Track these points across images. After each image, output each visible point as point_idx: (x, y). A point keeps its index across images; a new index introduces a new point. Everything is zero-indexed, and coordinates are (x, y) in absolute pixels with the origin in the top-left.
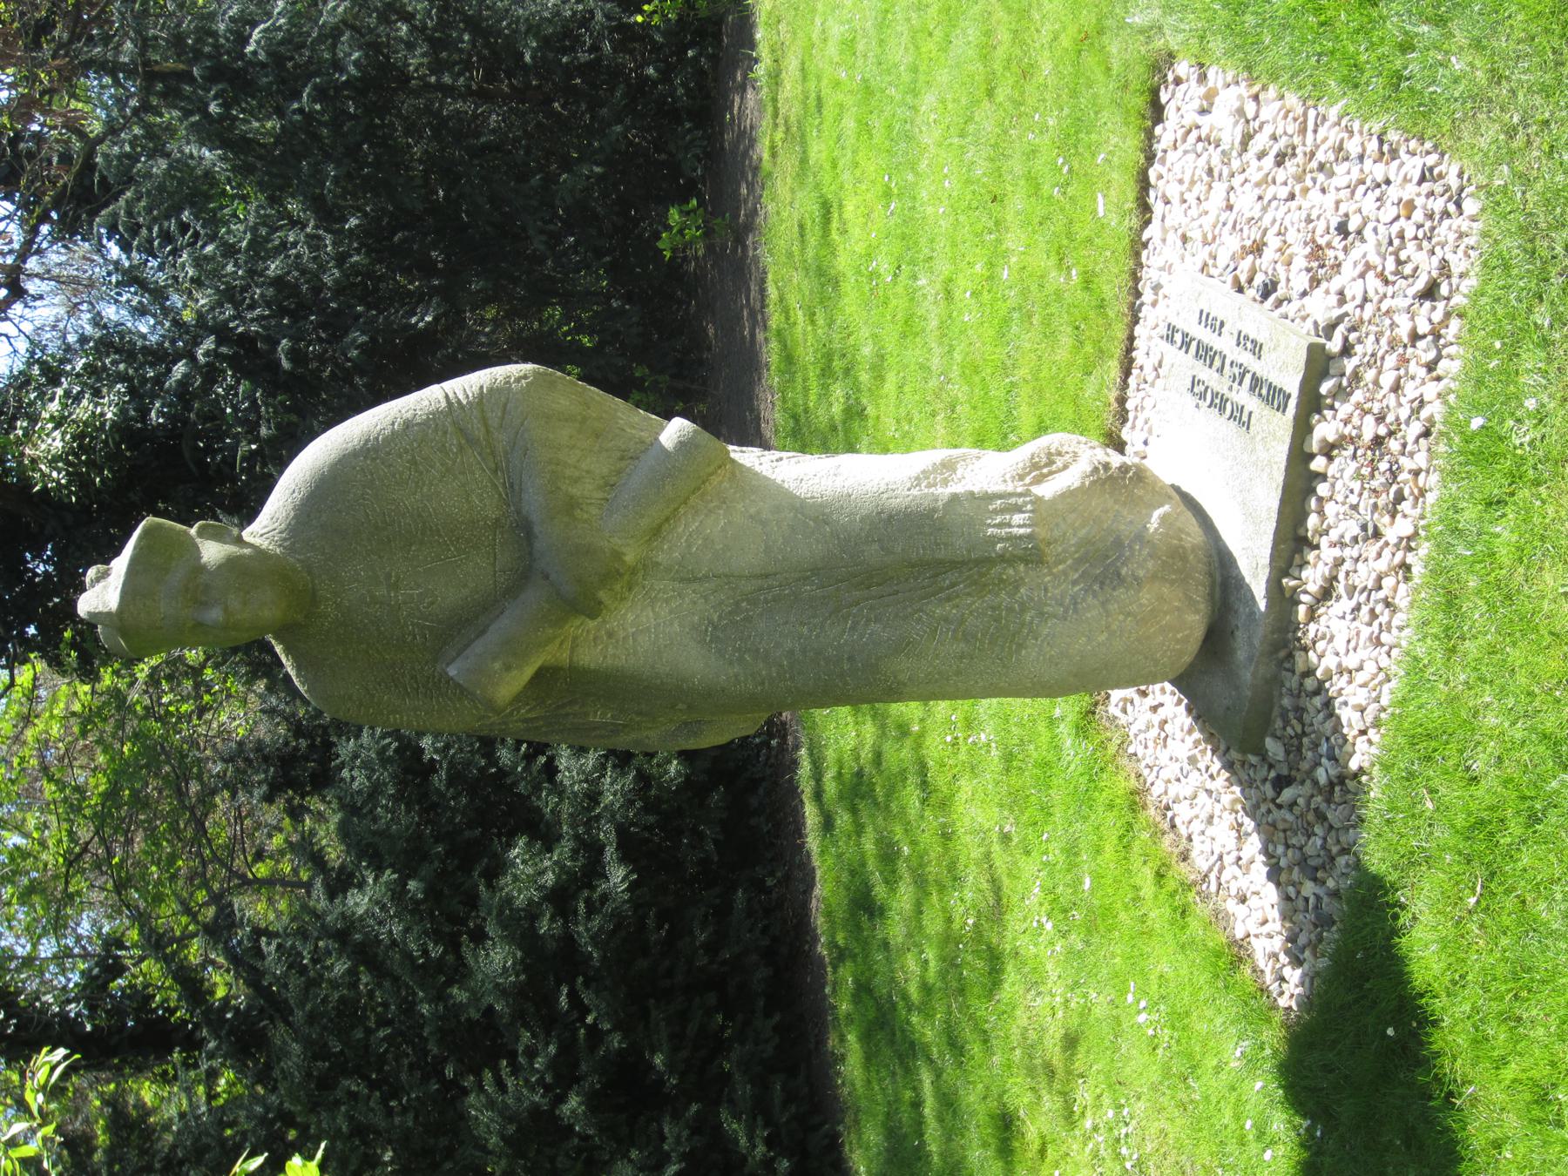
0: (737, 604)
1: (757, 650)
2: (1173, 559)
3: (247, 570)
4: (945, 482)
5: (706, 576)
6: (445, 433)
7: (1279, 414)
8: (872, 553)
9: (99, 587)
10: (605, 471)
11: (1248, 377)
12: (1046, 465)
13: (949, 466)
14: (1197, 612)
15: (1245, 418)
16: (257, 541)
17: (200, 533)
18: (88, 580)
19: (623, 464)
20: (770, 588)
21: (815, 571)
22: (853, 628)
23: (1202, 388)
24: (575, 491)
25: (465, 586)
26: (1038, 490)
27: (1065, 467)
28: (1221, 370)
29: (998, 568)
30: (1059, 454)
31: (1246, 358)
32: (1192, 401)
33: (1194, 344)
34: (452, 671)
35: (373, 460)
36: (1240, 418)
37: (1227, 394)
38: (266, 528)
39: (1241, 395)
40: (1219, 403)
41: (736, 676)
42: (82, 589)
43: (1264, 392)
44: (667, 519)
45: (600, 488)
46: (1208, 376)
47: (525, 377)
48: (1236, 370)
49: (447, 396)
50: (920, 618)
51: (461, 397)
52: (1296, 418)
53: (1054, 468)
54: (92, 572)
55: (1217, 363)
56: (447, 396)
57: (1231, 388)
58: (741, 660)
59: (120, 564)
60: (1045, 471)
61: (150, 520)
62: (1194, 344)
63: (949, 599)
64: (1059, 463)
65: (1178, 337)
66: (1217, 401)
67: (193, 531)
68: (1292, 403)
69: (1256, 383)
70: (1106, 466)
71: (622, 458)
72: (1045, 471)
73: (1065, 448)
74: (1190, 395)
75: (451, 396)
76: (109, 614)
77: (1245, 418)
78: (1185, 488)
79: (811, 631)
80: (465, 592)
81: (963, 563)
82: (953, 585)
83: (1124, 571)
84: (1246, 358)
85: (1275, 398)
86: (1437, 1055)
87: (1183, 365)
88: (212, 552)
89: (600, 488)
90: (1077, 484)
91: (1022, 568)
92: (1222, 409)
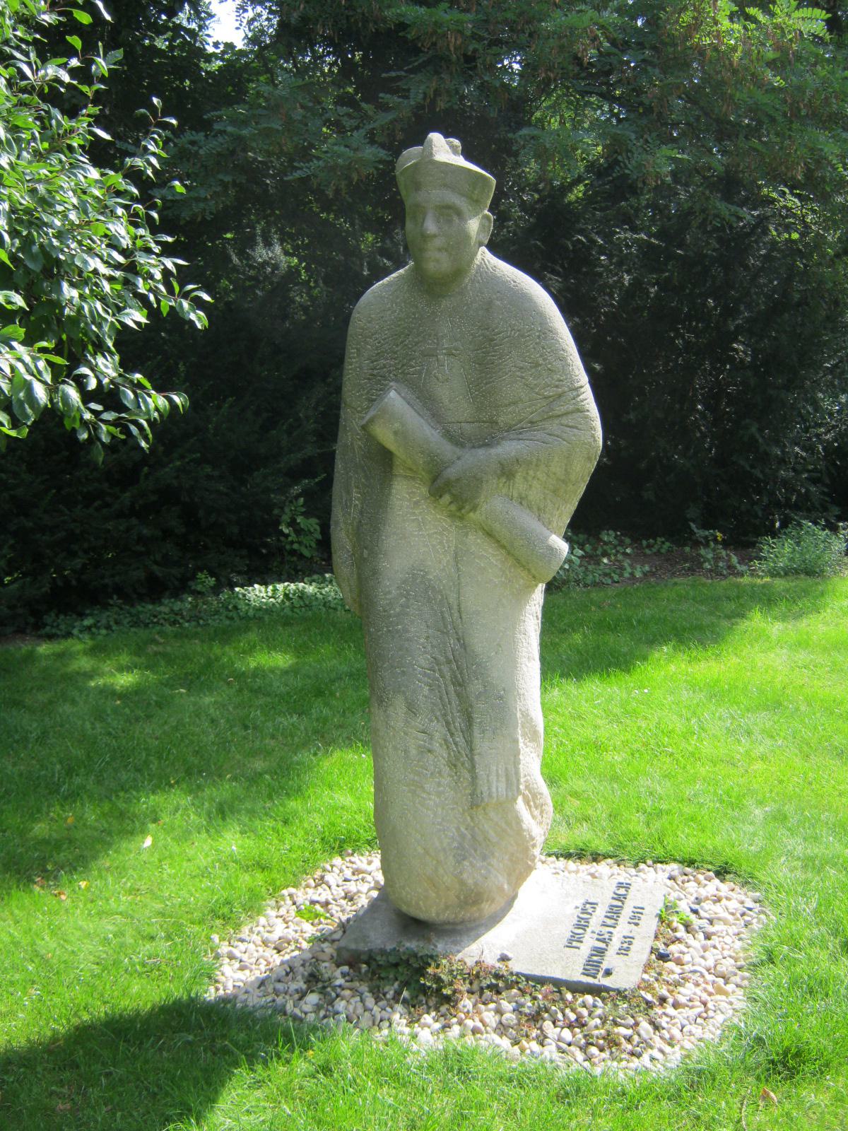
0: (440, 591)
1: (408, 607)
2: (473, 898)
3: (460, 246)
4: (524, 735)
5: (458, 569)
6: (557, 387)
7: (581, 971)
8: (475, 687)
9: (447, 147)
10: (531, 498)
11: (602, 945)
12: (535, 803)
13: (533, 736)
14: (438, 914)
15: (575, 944)
16: (479, 257)
17: (486, 217)
18: (451, 139)
19: (535, 509)
20: (451, 615)
21: (464, 646)
22: (425, 675)
23: (590, 911)
24: (519, 477)
25: (450, 401)
26: (520, 800)
27: (533, 817)
28: (604, 925)
29: (467, 775)
30: (542, 812)
31: (616, 943)
32: (580, 903)
33: (620, 904)
34: (393, 394)
35: (539, 337)
36: (574, 941)
37: (589, 930)
38: (485, 257)
39: (589, 942)
40: (582, 924)
41: (389, 592)
42: (446, 136)
43: (595, 958)
44: (498, 542)
45: (520, 495)
46: (601, 912)
47: (595, 441)
48: (607, 936)
49: (582, 387)
50: (432, 721)
51: (581, 397)
52: (580, 982)
53: (533, 809)
54: (457, 142)
55: (609, 922)
56: (582, 387)
57: (593, 932)
58: (402, 595)
59: (461, 161)
60: (532, 803)
61: (494, 181)
62: (620, 904)
63: (446, 740)
64: (536, 813)
65: (622, 891)
66: (583, 923)
67: (486, 212)
68: (590, 980)
69: (600, 952)
70: (534, 846)
71: (539, 509)
72: (532, 803)
73: (545, 816)
74: (583, 901)
75: (582, 390)
76: (431, 154)
77: (575, 944)
78: (516, 903)
79: (422, 644)
80: (446, 401)
81: (472, 750)
82: (456, 744)
83: (466, 863)
84: (616, 943)
85: (592, 966)
86: (29, 1040)
87: (604, 900)
88: (474, 225)
89: (520, 495)
90: (524, 826)
91: (468, 791)
92: (578, 926)
